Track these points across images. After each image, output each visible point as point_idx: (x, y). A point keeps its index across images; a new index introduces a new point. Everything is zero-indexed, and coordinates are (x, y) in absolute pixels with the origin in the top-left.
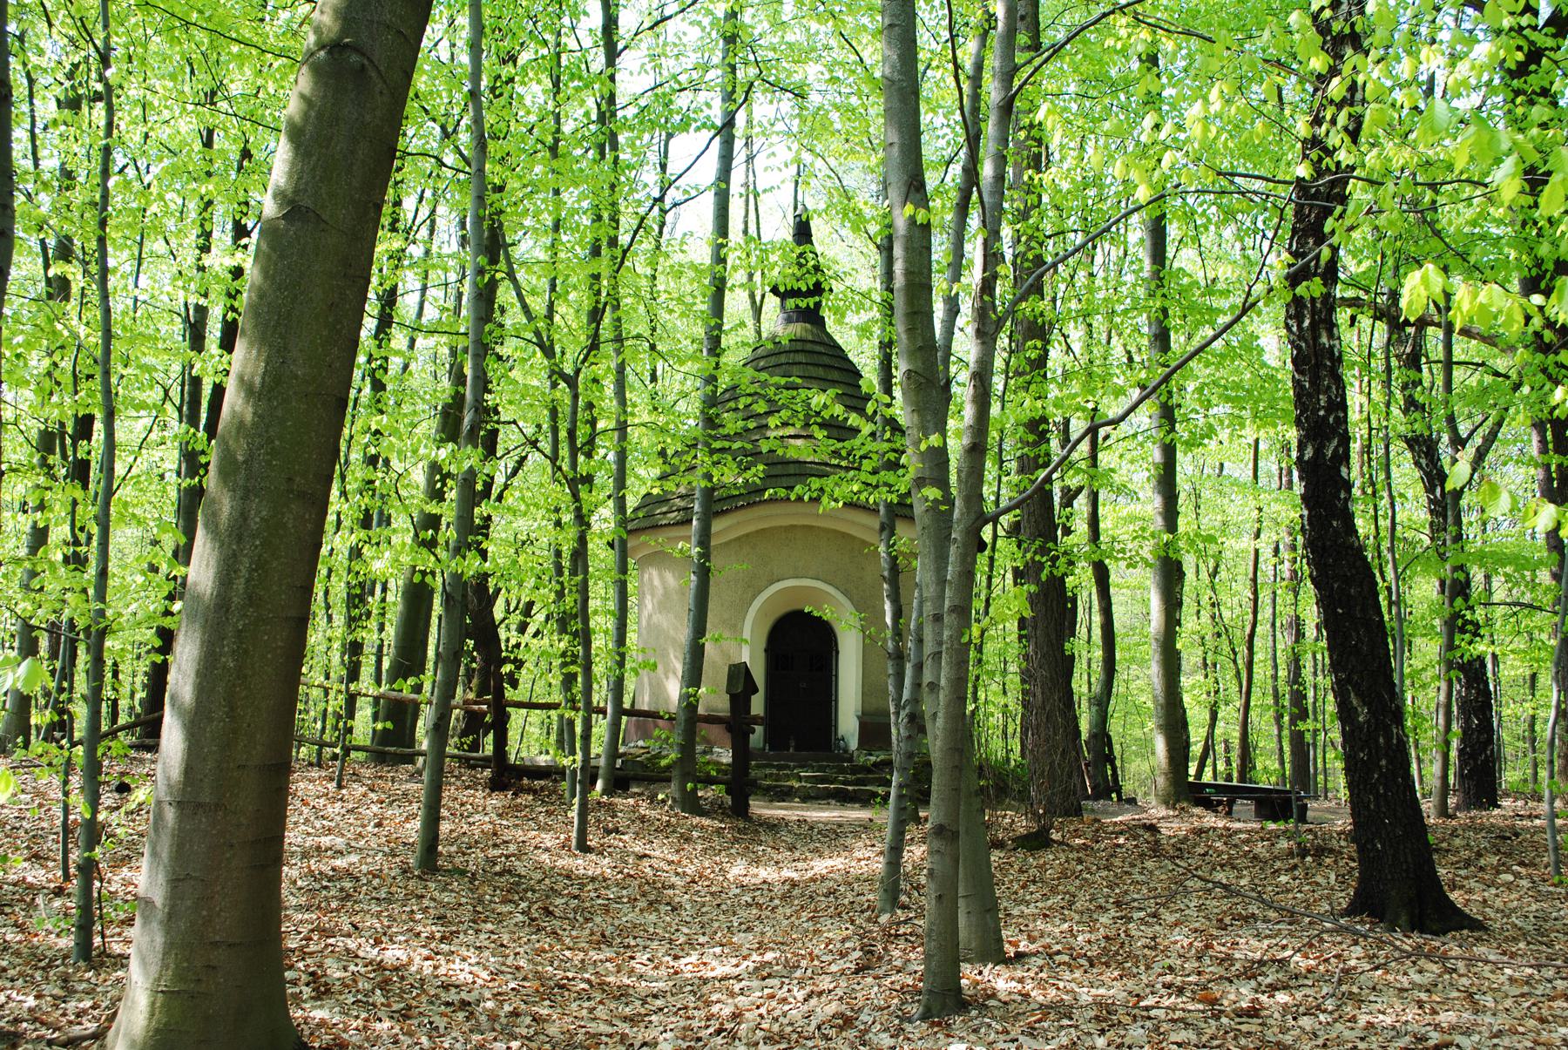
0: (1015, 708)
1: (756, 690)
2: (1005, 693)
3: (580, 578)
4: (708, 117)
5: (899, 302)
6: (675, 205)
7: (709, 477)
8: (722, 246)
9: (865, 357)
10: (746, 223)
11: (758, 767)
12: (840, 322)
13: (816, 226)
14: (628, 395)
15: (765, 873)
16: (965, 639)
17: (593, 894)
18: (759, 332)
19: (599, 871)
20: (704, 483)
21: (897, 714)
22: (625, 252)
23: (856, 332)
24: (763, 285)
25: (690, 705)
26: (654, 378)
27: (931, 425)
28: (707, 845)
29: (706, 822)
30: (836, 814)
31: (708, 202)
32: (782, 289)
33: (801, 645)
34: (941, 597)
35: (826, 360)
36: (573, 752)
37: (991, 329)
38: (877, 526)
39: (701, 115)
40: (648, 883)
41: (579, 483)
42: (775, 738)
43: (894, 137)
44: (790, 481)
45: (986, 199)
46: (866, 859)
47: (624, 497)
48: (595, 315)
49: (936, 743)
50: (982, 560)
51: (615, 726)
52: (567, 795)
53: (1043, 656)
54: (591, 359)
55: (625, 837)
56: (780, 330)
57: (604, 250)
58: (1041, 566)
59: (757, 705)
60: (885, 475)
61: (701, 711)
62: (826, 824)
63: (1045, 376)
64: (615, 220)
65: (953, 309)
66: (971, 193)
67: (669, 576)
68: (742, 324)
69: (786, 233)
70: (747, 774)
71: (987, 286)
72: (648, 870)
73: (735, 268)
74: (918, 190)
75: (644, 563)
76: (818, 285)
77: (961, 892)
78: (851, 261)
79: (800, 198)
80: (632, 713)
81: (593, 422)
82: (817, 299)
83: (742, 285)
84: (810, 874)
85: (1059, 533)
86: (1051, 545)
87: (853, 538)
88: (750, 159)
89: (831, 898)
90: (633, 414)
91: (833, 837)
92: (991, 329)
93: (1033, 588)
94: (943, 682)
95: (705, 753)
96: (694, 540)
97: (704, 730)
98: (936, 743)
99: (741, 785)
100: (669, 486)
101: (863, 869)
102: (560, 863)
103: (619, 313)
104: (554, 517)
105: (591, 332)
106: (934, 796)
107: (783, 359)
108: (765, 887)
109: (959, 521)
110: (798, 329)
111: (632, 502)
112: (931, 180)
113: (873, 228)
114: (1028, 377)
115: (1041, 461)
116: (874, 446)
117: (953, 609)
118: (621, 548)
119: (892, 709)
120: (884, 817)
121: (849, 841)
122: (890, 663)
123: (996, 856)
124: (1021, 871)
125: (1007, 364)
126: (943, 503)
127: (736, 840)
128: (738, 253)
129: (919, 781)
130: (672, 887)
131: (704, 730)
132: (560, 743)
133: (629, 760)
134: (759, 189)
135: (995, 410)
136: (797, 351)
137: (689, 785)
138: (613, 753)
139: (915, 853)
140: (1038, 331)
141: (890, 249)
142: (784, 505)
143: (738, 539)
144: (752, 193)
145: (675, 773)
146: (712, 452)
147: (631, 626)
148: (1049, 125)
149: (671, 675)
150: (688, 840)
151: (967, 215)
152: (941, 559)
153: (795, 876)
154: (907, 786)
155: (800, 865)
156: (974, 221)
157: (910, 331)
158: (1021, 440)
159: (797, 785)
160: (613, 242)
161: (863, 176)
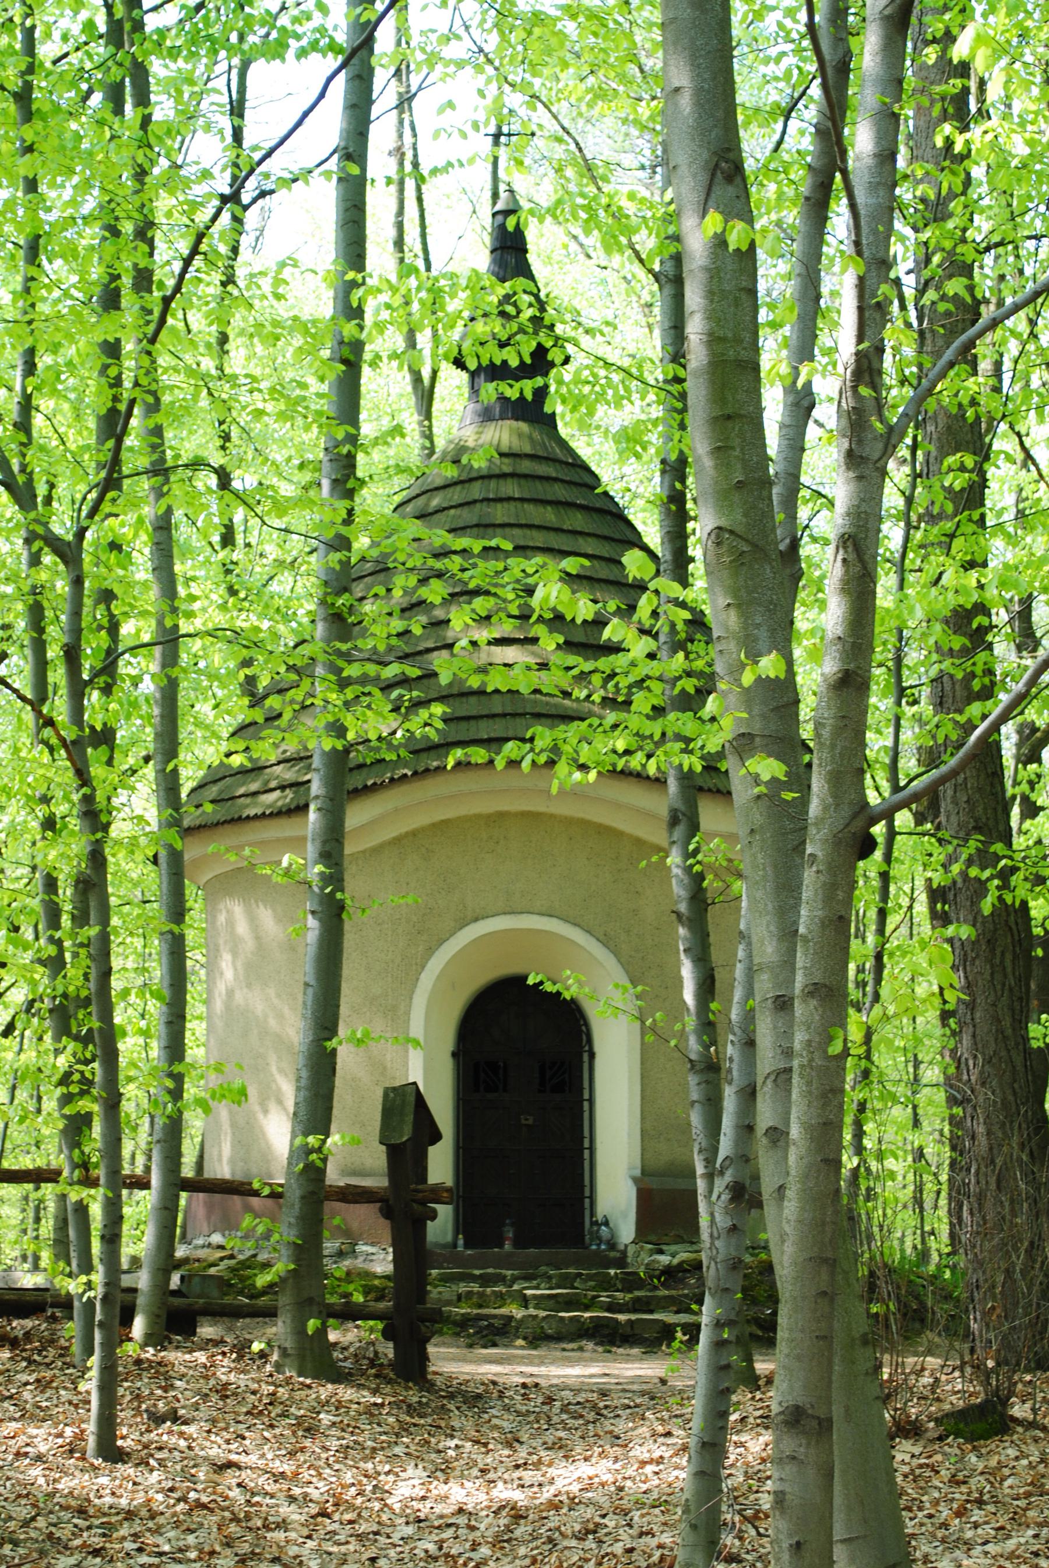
0: (939, 1154)
1: (436, 1136)
2: (916, 1123)
3: (93, 931)
4: (322, 30)
5: (697, 390)
6: (263, 194)
7: (338, 729)
8: (354, 284)
9: (633, 485)
10: (400, 226)
11: (445, 1279)
12: (584, 426)
13: (542, 242)
14: (178, 568)
15: (460, 1493)
16: (836, 1048)
17: (129, 1546)
18: (429, 436)
19: (140, 1498)
20: (328, 744)
21: (710, 1177)
22: (167, 301)
23: (620, 444)
24: (434, 355)
25: (312, 1172)
26: (228, 539)
27: (763, 634)
28: (348, 1440)
29: (347, 1393)
30: (594, 1369)
31: (323, 198)
32: (472, 365)
33: (521, 1048)
34: (788, 963)
35: (560, 492)
36: (87, 1267)
37: (874, 450)
38: (664, 812)
39: (309, 26)
40: (235, 1519)
41: (86, 746)
42: (475, 1227)
43: (682, 77)
44: (496, 729)
45: (861, 198)
46: (653, 1463)
47: (175, 771)
48: (113, 425)
49: (785, 1233)
50: (871, 866)
51: (167, 1209)
52: (76, 1348)
53: (988, 1061)
54: (106, 507)
55: (191, 1429)
56: (469, 435)
57: (128, 298)
58: (981, 888)
59: (441, 1165)
60: (677, 721)
61: (334, 1177)
62: (577, 1391)
63: (982, 521)
64: (145, 232)
65: (802, 404)
66: (833, 177)
67: (266, 916)
68: (398, 430)
69: (479, 257)
70: (422, 1295)
71: (867, 368)
72: (235, 1493)
73: (380, 327)
74: (729, 179)
75: (222, 886)
76: (541, 351)
77: (839, 1532)
78: (606, 309)
79: (501, 174)
80: (198, 1185)
81: (113, 628)
82: (539, 381)
83: (394, 356)
84: (548, 1493)
85: (1016, 812)
86: (998, 847)
87: (618, 834)
88: (405, 102)
89: (590, 1543)
90: (190, 615)
91: (590, 1417)
92: (874, 450)
93: (965, 932)
94: (795, 1131)
95: (340, 1254)
96: (311, 849)
97: (338, 1215)
98: (785, 1233)
99: (410, 1321)
100: (266, 750)
101: (648, 1481)
102: (65, 1484)
103: (159, 418)
104: (41, 811)
105: (106, 456)
106: (781, 1334)
107: (476, 491)
108: (462, 1520)
109: (819, 822)
110: (505, 434)
111: (189, 777)
112: (755, 144)
113: (647, 241)
114: (949, 526)
115: (976, 685)
116: (654, 668)
117: (814, 991)
118: (175, 870)
119: (700, 1169)
120: (688, 1371)
121: (621, 1426)
122: (693, 1080)
123: (905, 1452)
124: (955, 1481)
125: (909, 500)
126: (788, 786)
127: (405, 1429)
128: (385, 297)
129: (754, 1301)
130: (283, 1525)
131: (338, 1215)
132: (61, 1246)
133: (196, 1274)
134: (425, 169)
135: (886, 582)
136: (503, 476)
137: (312, 1324)
138: (165, 1261)
139: (751, 1447)
140: (968, 435)
141: (678, 282)
142: (484, 773)
143: (397, 841)
144: (412, 172)
145: (284, 1300)
146: (343, 684)
147: (195, 1007)
148: (979, 66)
149: (273, 1106)
150: (310, 1431)
151: (826, 219)
152: (787, 890)
153: (517, 1496)
154: (731, 1323)
155: (529, 1476)
156: (839, 222)
157: (720, 451)
158: (938, 649)
159: (518, 1313)
160: (144, 279)
161: (626, 144)
